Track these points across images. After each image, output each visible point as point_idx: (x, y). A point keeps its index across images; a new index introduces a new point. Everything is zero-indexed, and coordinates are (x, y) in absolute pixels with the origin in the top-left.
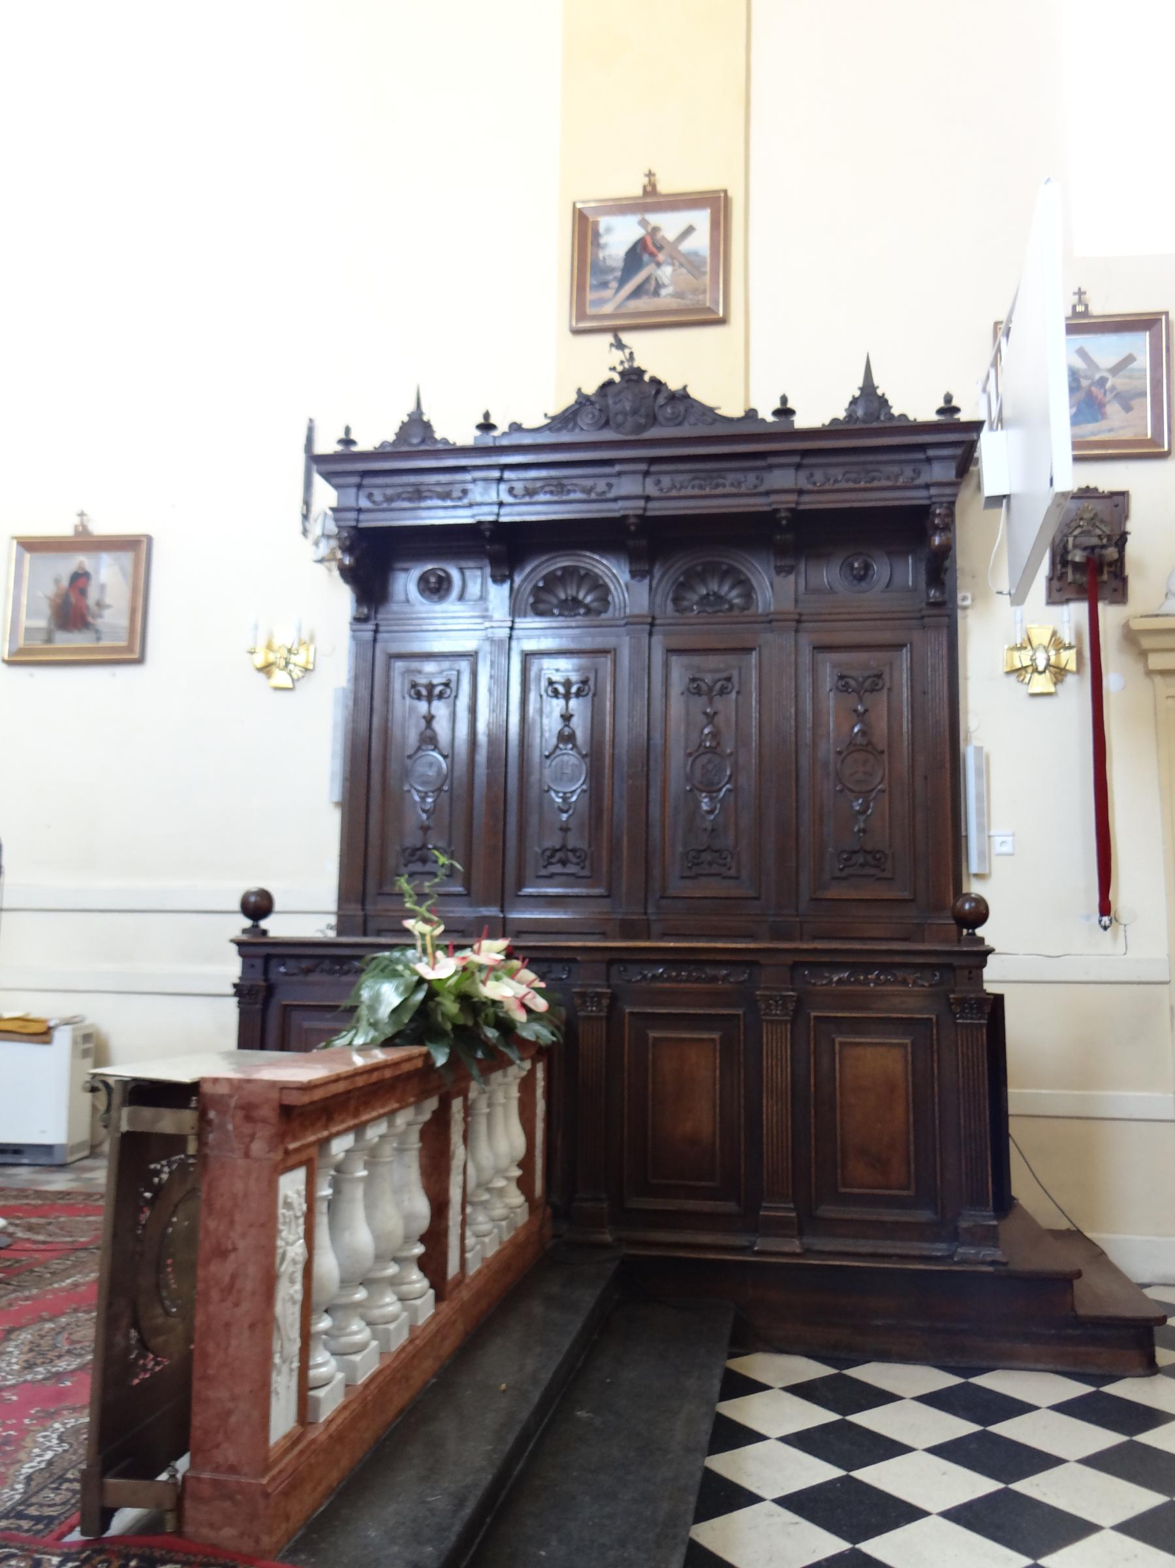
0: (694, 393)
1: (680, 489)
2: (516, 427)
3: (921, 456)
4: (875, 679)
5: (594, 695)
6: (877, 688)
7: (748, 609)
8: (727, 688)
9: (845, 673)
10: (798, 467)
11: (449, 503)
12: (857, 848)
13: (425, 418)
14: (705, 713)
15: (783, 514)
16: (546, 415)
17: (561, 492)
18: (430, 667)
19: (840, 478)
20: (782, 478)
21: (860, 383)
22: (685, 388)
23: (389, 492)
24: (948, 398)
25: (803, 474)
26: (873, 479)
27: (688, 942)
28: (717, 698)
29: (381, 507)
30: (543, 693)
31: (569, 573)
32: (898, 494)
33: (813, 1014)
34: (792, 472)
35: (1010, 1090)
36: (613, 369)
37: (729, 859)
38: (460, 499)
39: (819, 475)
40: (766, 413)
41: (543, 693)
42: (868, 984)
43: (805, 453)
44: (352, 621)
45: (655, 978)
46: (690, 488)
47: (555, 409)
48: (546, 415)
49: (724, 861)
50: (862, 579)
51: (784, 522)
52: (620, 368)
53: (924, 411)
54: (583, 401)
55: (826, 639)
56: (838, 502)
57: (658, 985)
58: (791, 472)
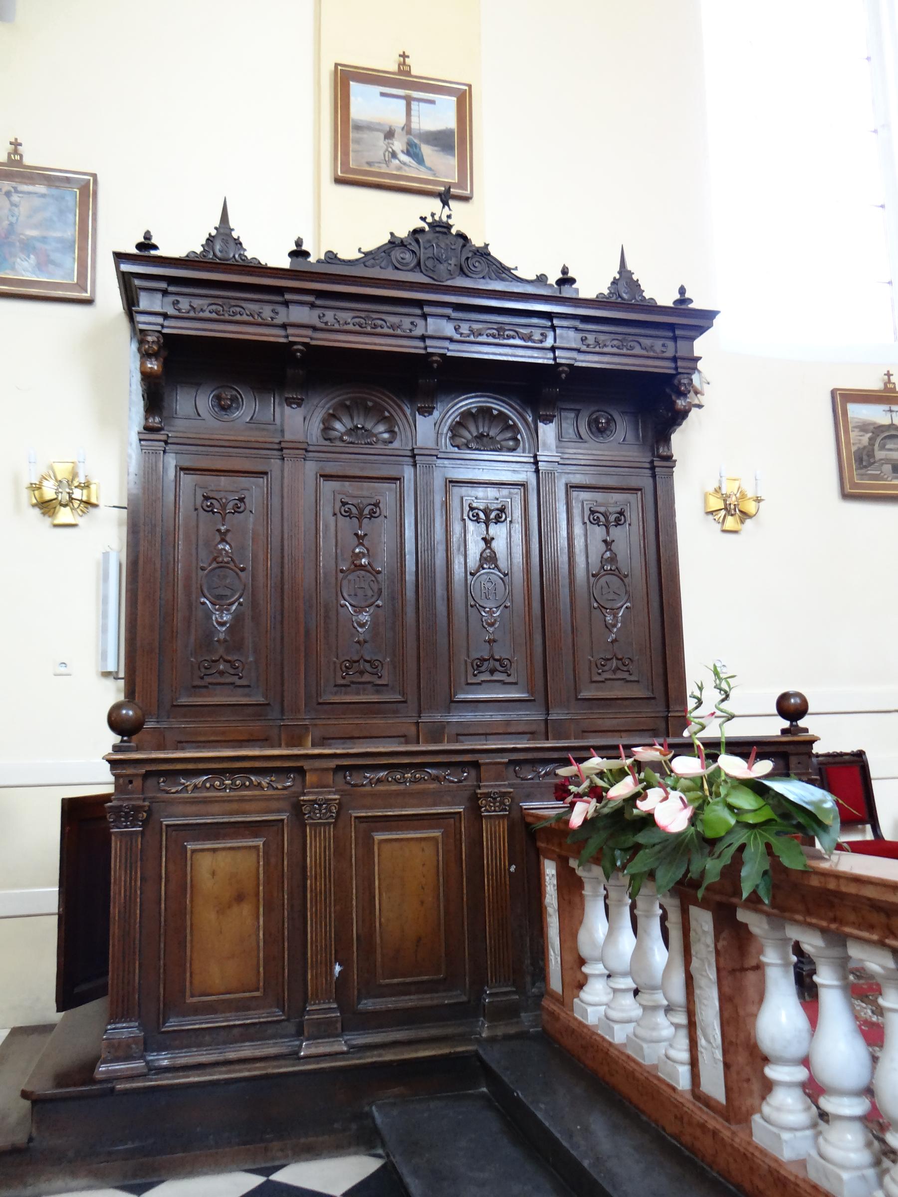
0: (494, 251)
1: (603, 347)
2: (331, 257)
3: (279, 298)
4: (499, 512)
5: (511, 522)
6: (239, 510)
7: (391, 442)
8: (375, 513)
9: (211, 494)
10: (313, 306)
11: (530, 344)
12: (356, 658)
13: (235, 235)
14: (356, 535)
15: (435, 358)
16: (360, 250)
17: (500, 336)
18: (480, 492)
19: (608, 343)
20: (299, 314)
21: (217, 223)
22: (487, 245)
23: (476, 326)
24: (147, 236)
25: (317, 312)
26: (235, 314)
27: (213, 752)
28: (365, 521)
29: (467, 339)
30: (466, 518)
31: (485, 412)
32: (221, 327)
33: (166, 822)
34: (159, 296)
35: (56, 889)
36: (423, 219)
37: (380, 668)
38: (541, 342)
39: (329, 315)
40: (553, 277)
41: (586, 520)
42: (405, 782)
43: (171, 280)
44: (142, 430)
45: (379, 781)
46: (351, 325)
47: (370, 245)
48: (360, 250)
49: (375, 670)
50: (224, 408)
51: (435, 365)
52: (429, 220)
53: (666, 298)
54: (394, 243)
55: (331, 468)
56: (500, 354)
57: (381, 788)
58: (306, 309)
